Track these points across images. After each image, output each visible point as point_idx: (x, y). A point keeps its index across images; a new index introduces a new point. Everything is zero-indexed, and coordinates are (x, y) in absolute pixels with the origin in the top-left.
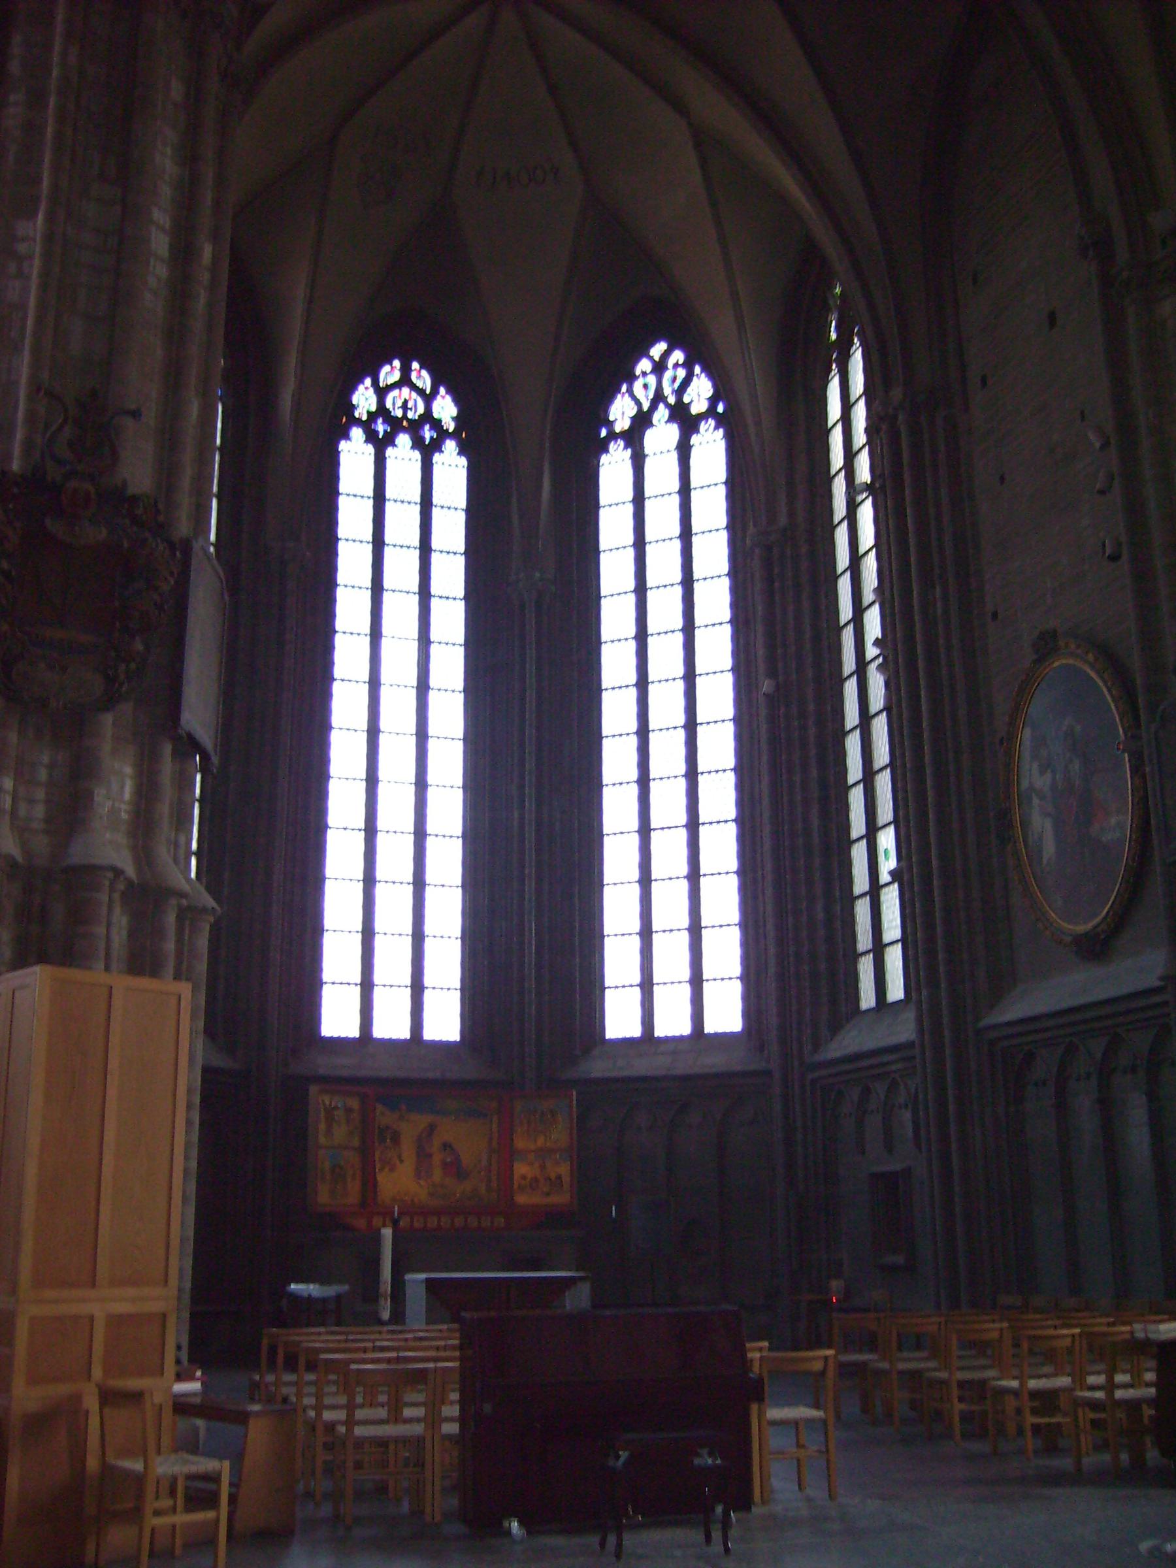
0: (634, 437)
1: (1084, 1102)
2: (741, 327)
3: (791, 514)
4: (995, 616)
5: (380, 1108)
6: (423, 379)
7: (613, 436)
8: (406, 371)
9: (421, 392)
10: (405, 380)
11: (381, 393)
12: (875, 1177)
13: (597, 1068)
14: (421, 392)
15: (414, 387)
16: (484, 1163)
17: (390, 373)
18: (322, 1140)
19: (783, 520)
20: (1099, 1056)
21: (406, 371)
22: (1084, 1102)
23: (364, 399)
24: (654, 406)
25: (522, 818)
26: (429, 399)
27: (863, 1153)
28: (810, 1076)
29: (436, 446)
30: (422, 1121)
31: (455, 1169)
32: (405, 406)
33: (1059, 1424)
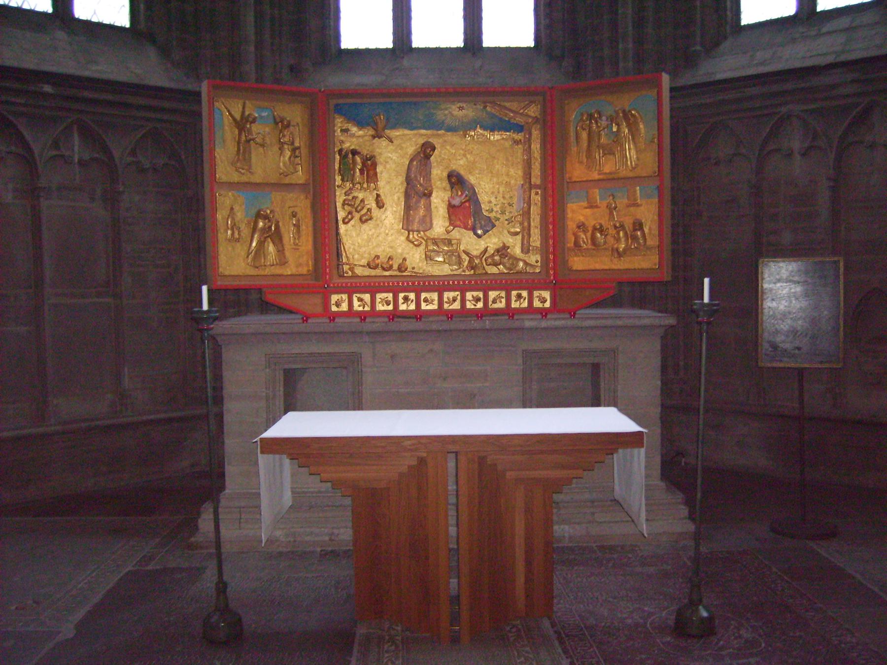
5: (339, 122)
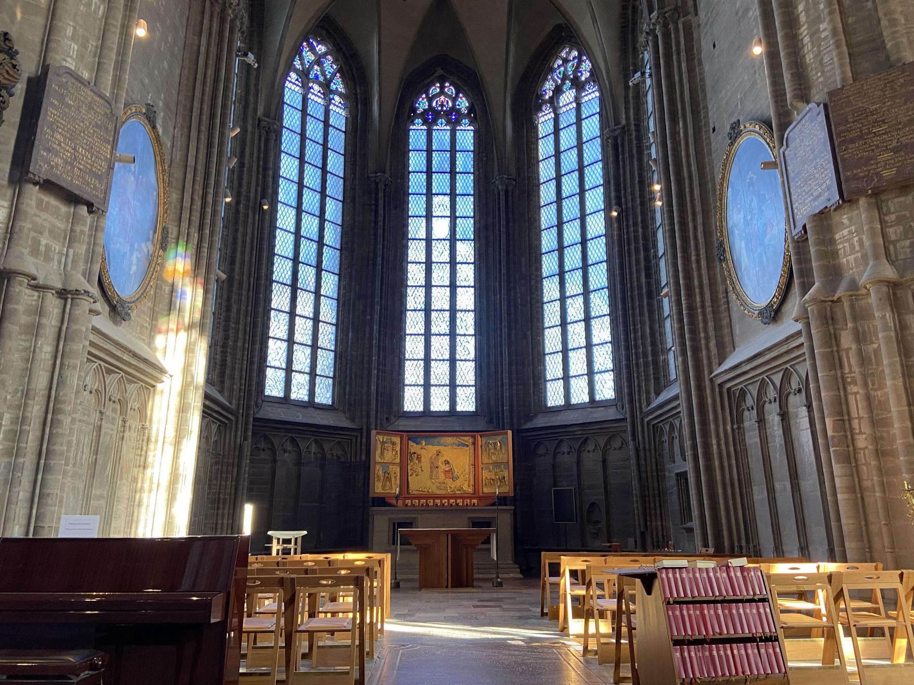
0: (553, 102)
1: (773, 418)
2: (594, 20)
3: (627, 118)
4: (714, 130)
5: (411, 443)
6: (450, 90)
7: (545, 102)
8: (442, 88)
9: (450, 97)
10: (442, 92)
11: (430, 100)
12: (677, 474)
13: (541, 421)
14: (450, 97)
15: (446, 95)
16: (467, 471)
17: (435, 89)
18: (378, 459)
19: (624, 122)
20: (778, 386)
21: (442, 88)
22: (773, 418)
23: (422, 104)
24: (563, 83)
25: (500, 298)
26: (454, 100)
27: (674, 462)
28: (646, 420)
29: (458, 122)
30: (433, 449)
31: (450, 473)
32: (442, 106)
33: (402, 654)
